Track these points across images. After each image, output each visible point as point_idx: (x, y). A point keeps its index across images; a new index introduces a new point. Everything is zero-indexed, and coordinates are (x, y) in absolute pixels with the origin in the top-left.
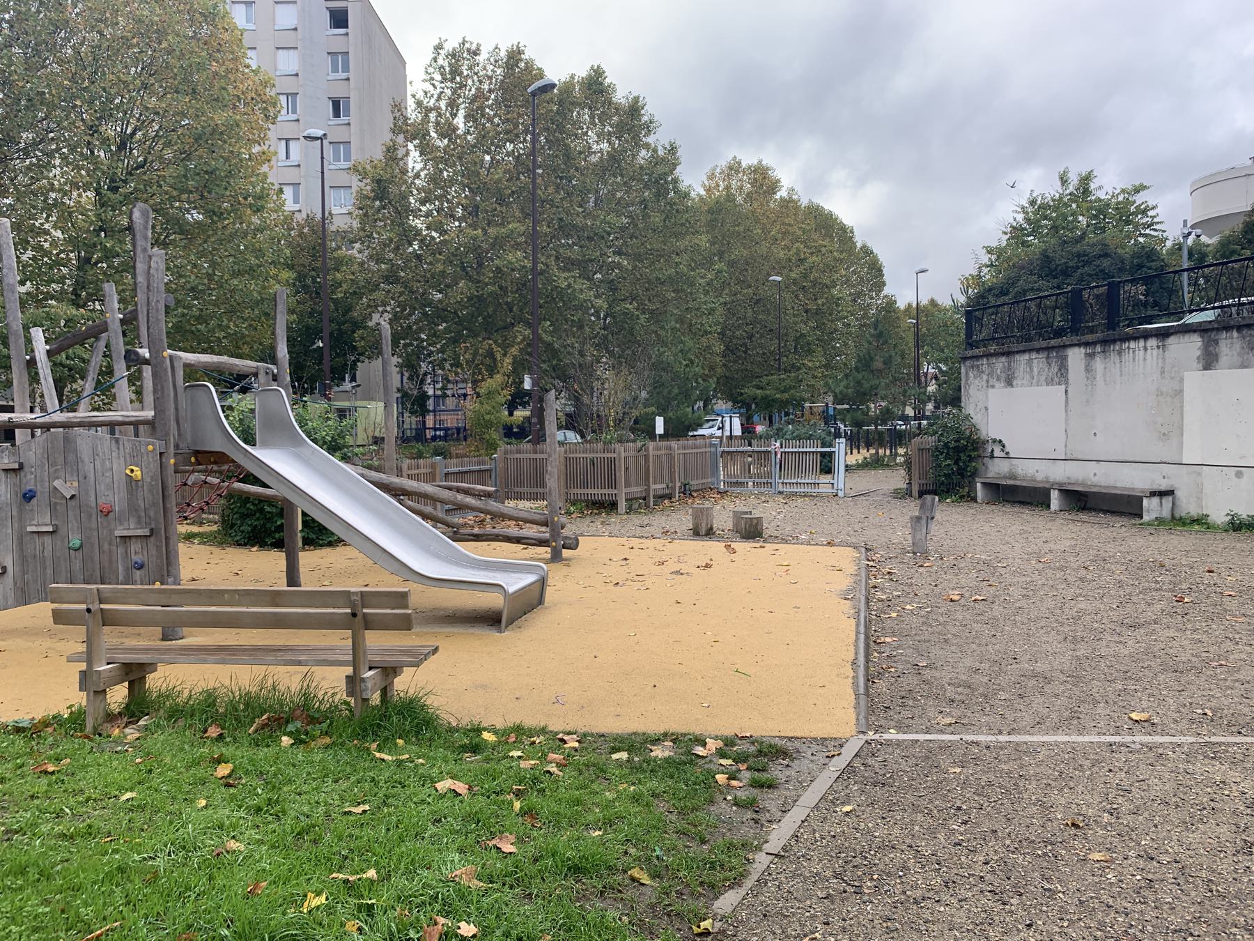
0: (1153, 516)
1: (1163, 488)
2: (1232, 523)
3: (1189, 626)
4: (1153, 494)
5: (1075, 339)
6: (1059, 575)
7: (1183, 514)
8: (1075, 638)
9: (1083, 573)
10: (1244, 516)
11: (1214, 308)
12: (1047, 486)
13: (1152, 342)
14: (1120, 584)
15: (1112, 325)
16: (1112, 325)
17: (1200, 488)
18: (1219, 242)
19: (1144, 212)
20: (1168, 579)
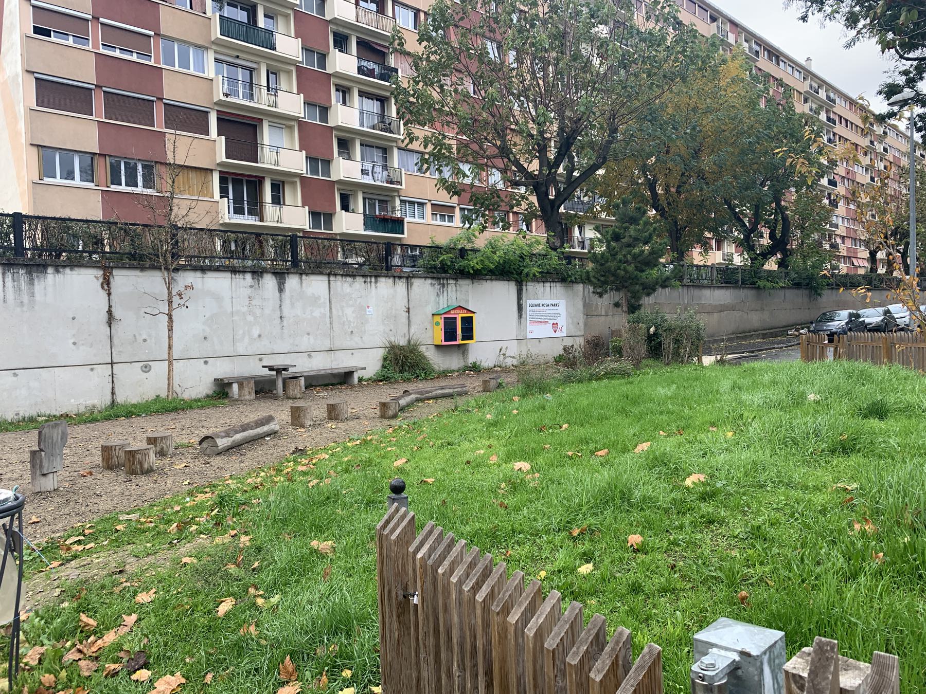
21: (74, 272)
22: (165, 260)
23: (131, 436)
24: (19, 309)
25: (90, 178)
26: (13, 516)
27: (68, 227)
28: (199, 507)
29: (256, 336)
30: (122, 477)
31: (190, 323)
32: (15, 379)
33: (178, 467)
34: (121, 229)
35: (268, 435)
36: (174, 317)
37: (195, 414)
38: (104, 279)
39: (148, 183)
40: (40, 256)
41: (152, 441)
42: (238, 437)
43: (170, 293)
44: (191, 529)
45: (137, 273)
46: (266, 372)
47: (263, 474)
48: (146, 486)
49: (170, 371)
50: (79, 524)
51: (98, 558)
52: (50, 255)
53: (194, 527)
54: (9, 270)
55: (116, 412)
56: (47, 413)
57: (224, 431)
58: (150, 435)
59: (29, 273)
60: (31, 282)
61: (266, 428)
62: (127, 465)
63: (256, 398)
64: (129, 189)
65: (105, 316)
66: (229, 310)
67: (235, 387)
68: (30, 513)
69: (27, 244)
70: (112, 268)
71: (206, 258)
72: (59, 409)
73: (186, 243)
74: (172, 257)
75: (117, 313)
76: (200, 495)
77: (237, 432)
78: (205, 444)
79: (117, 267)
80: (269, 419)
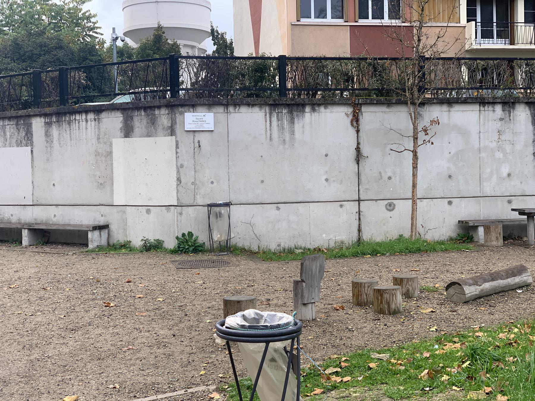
0: (96, 244)
1: (102, 223)
2: (145, 246)
3: (112, 324)
4: (95, 228)
5: (37, 110)
6: (24, 296)
7: (115, 242)
8: (31, 346)
9: (42, 293)
10: (152, 241)
11: (130, 94)
12: (19, 226)
13: (91, 116)
14: (68, 299)
15: (63, 101)
16: (63, 101)
17: (125, 222)
18: (140, 47)
19: (88, 18)
20: (101, 290)
21: (328, 110)
22: (412, 94)
23: (380, 274)
24: (281, 147)
25: (340, 14)
26: (293, 340)
27: (323, 67)
28: (449, 357)
29: (505, 174)
30: (371, 316)
31: (435, 161)
32: (277, 212)
33: (424, 311)
34: (370, 64)
35: (520, 287)
36: (419, 154)
37: (439, 257)
38: (354, 116)
39: (395, 13)
40: (299, 95)
41: (398, 281)
42: (487, 286)
43: (415, 129)
44: (443, 379)
45: (384, 109)
46: (516, 215)
47: (516, 330)
48: (393, 326)
49: (414, 210)
50: (335, 356)
51: (355, 392)
52: (308, 93)
53: (445, 377)
54: (274, 110)
55: (361, 249)
56: (303, 246)
57: (472, 278)
58: (397, 275)
59: (291, 112)
60: (292, 122)
61: (517, 280)
62: (376, 304)
63: (504, 245)
64: (377, 22)
65: (352, 152)
66: (477, 146)
67: (481, 230)
68: (306, 338)
69: (289, 85)
70: (361, 104)
71: (452, 89)
72: (313, 243)
73: (433, 75)
74: (419, 91)
75: (365, 150)
76: (449, 344)
77: (486, 281)
78: (451, 290)
79: (366, 104)
80: (521, 270)
